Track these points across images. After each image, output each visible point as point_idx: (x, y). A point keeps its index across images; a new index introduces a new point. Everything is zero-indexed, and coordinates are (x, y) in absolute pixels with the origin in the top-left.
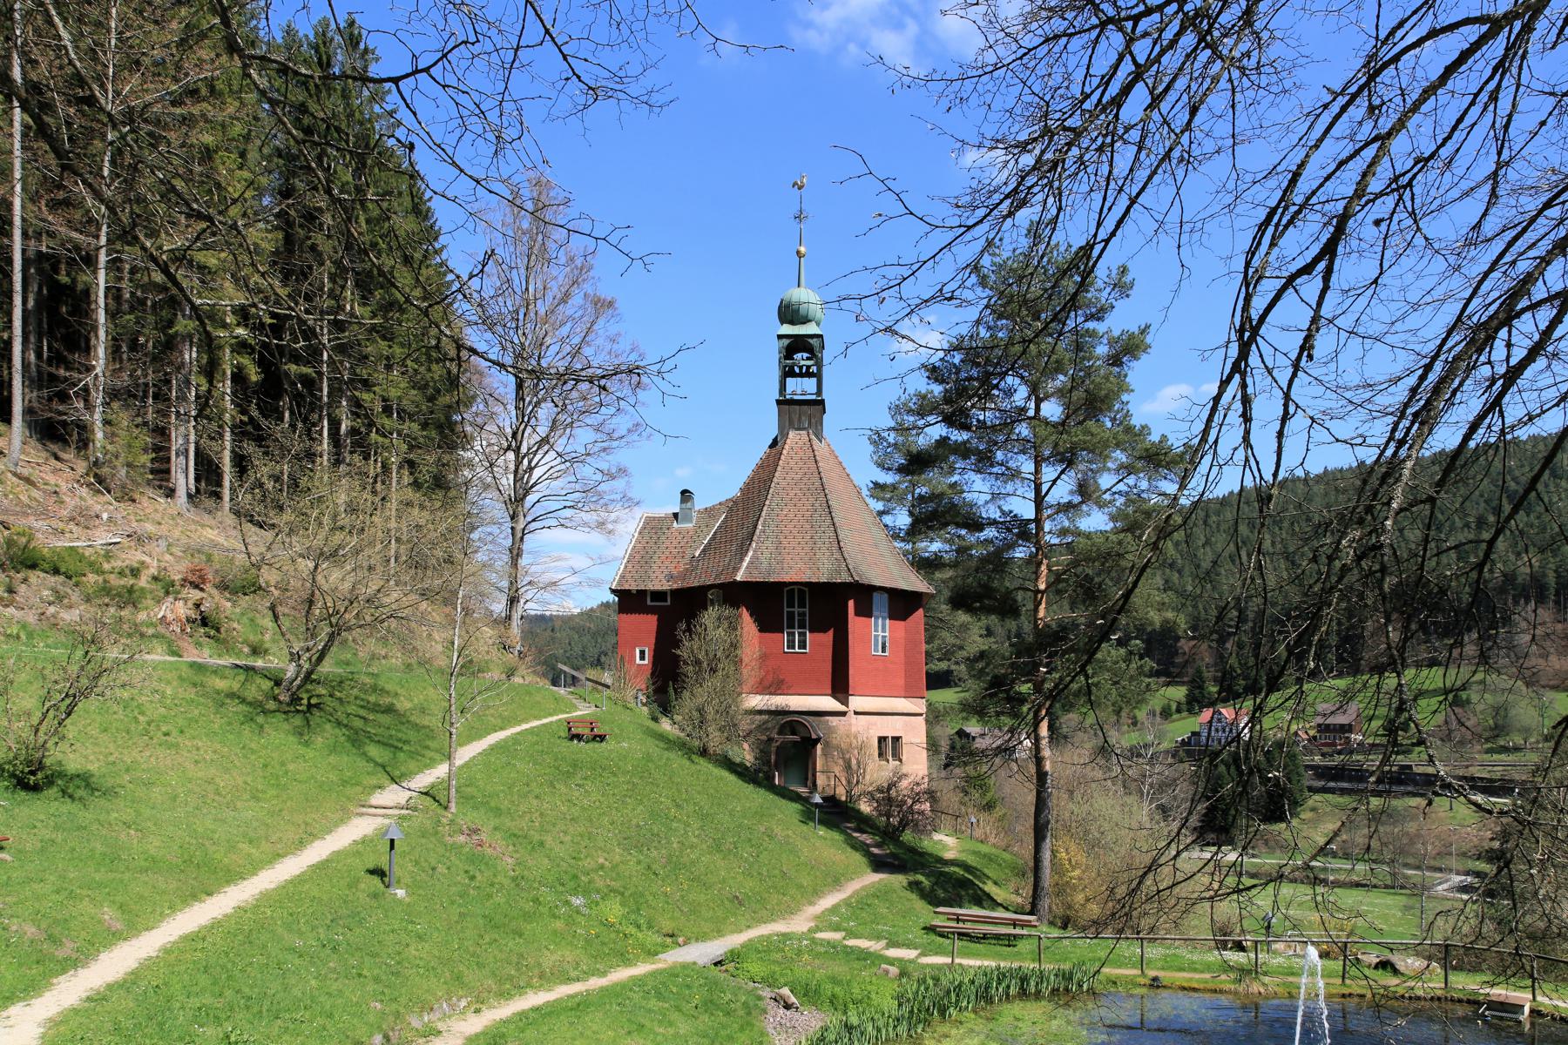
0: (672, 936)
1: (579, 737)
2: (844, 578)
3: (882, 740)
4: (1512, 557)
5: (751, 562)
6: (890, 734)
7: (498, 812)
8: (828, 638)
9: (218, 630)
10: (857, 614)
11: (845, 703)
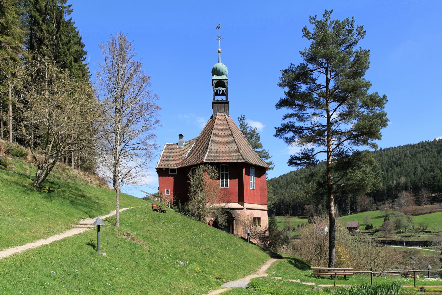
0: (220, 279)
1: (156, 210)
2: (242, 160)
4: (398, 179)
5: (208, 156)
7: (137, 229)
8: (236, 182)
9: (6, 166)
10: (246, 174)
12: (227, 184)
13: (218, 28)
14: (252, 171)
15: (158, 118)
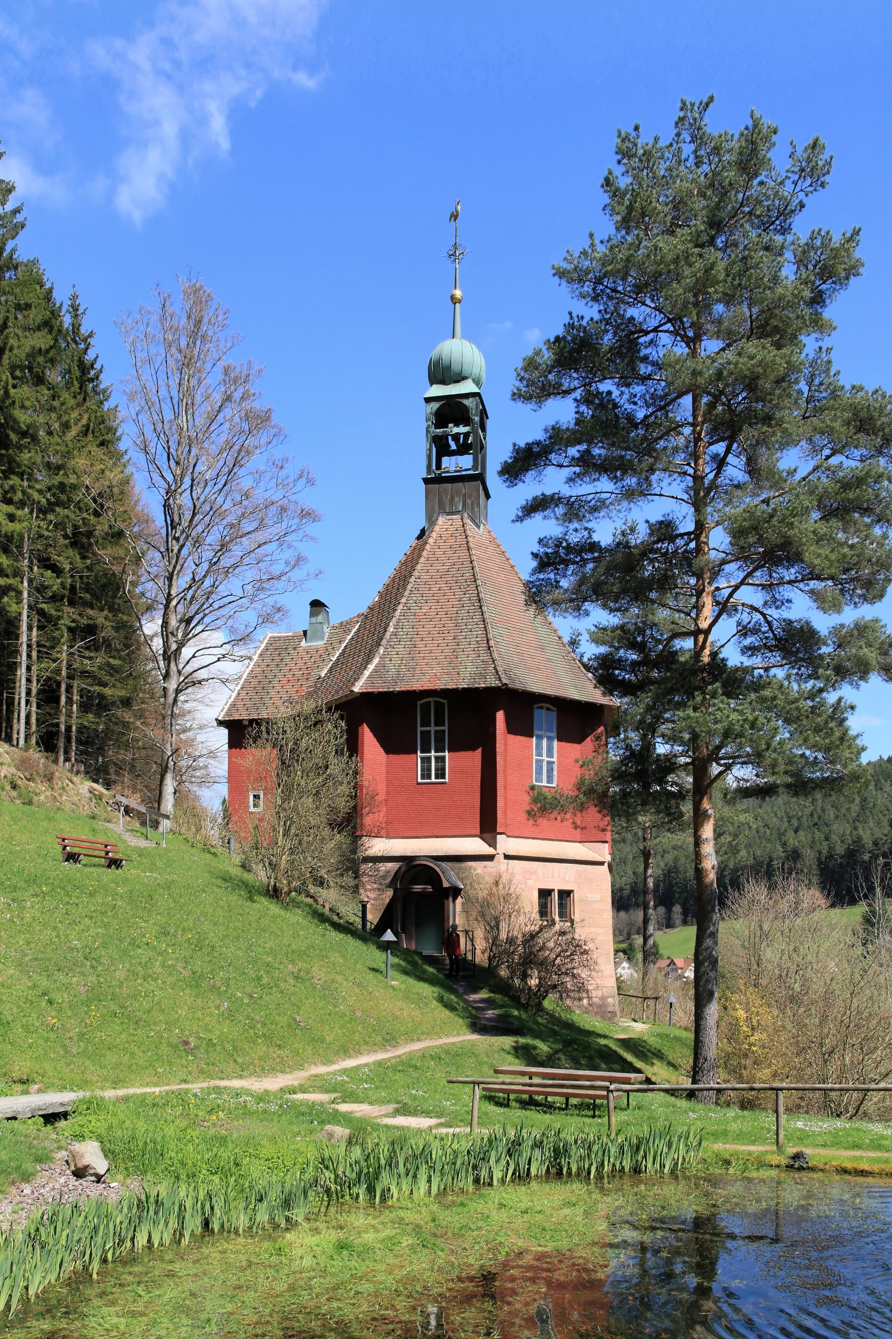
3: (545, 894)
5: (375, 671)
6: (557, 885)
11: (493, 844)
12: (444, 769)
13: (455, 216)
14: (543, 717)
15: (305, 548)
